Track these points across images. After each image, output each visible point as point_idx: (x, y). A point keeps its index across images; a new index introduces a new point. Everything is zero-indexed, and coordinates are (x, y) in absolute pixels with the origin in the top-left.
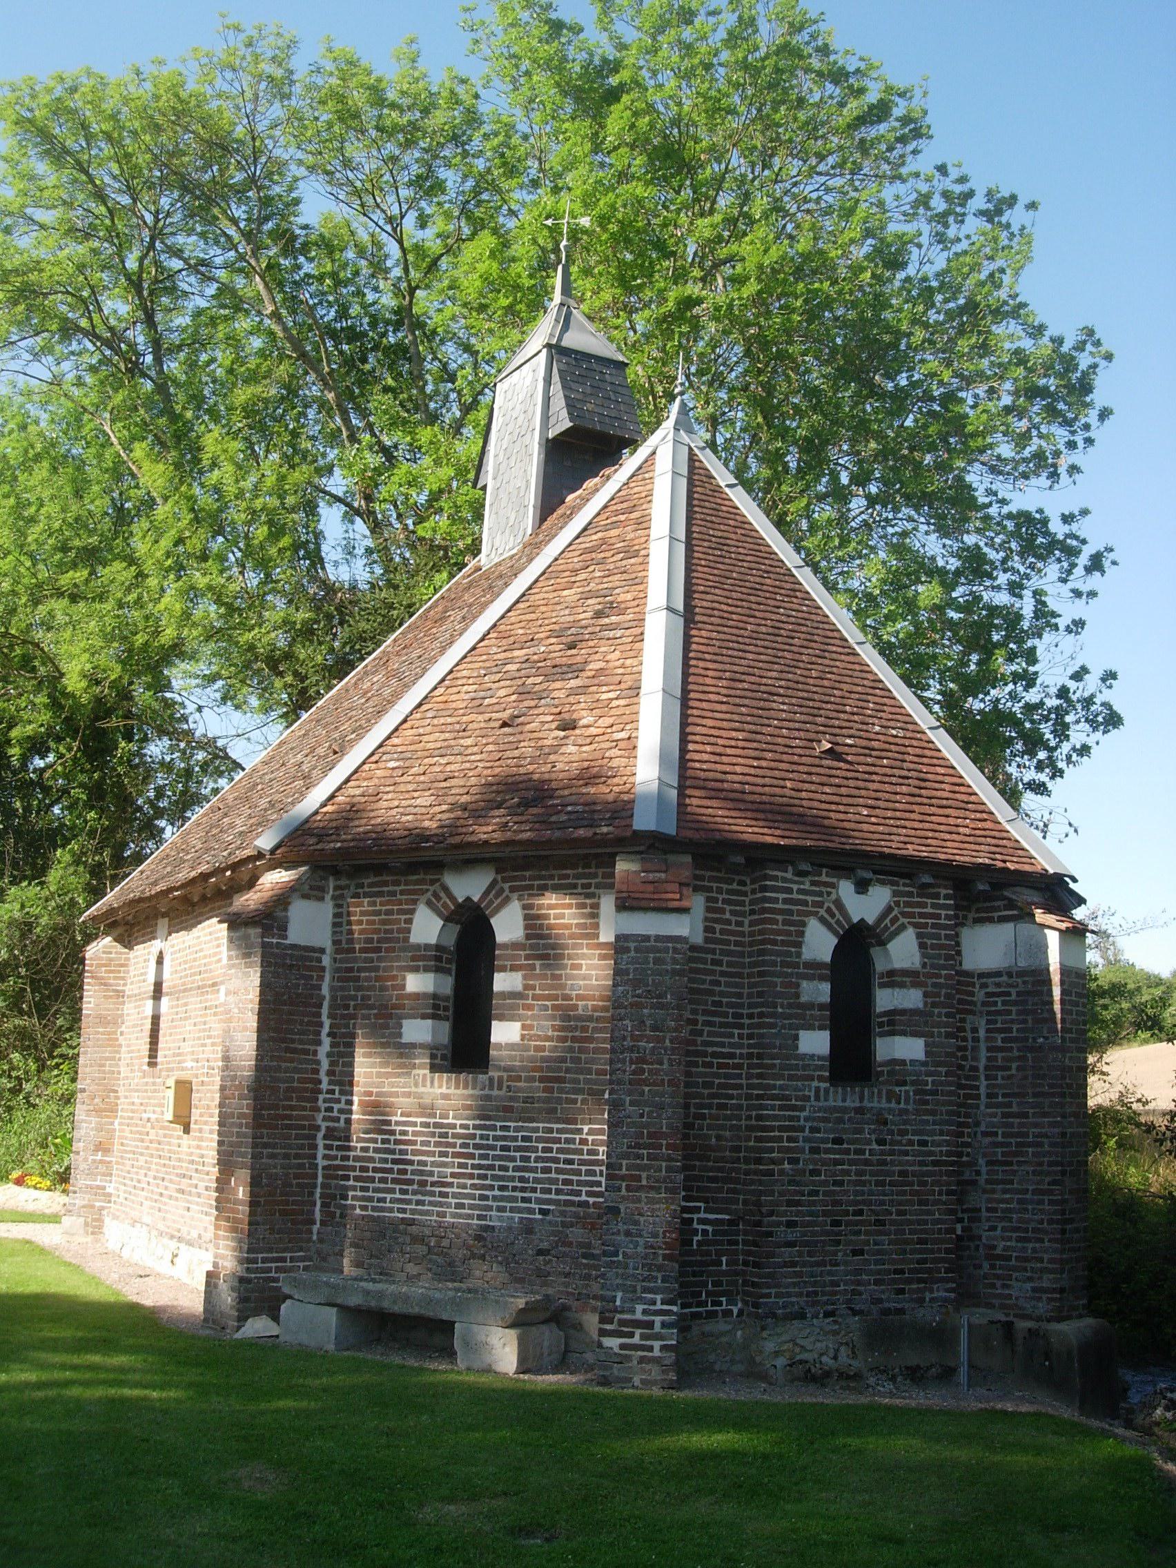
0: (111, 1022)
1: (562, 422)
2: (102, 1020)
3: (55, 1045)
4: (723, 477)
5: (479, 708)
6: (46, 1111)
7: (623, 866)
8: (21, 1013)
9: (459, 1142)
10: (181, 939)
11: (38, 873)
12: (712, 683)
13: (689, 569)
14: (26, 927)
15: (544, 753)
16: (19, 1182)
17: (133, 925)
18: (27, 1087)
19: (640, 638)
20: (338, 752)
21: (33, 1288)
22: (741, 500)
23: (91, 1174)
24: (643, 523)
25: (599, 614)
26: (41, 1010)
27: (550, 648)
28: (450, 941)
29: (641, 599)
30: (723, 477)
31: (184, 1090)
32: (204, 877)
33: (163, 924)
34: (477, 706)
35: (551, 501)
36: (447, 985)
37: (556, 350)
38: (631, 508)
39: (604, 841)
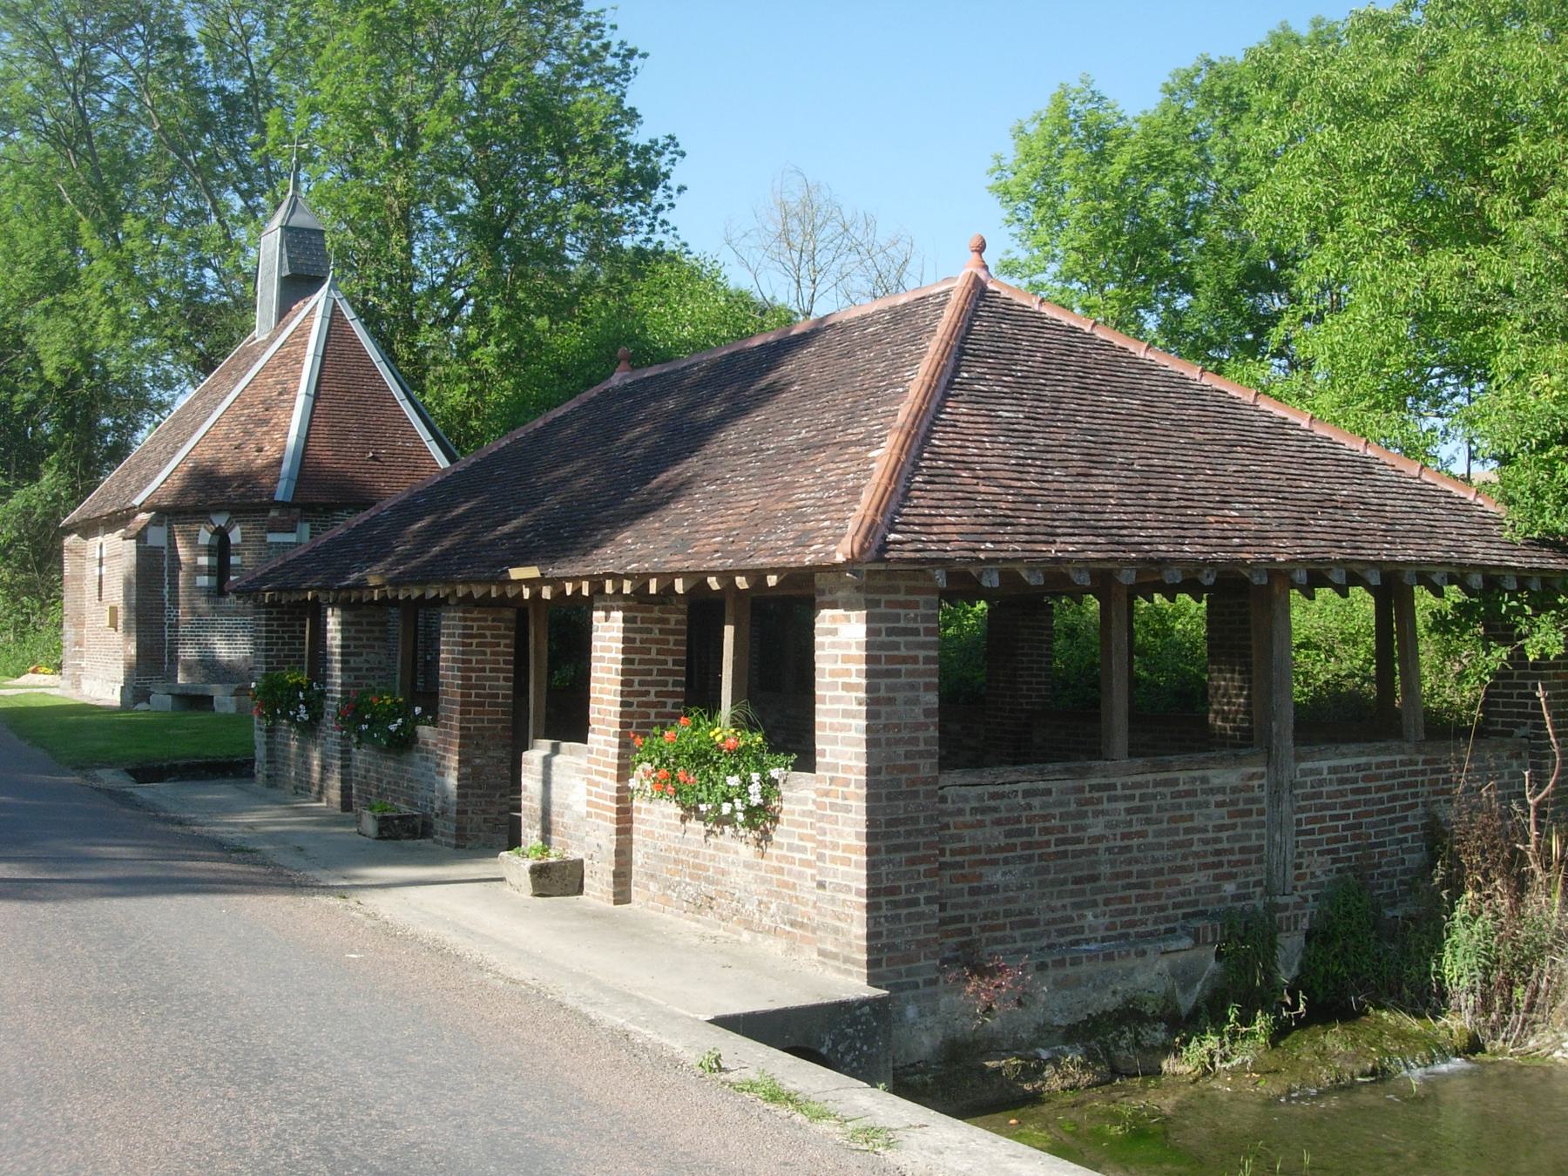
0: (80, 578)
1: (287, 273)
2: (75, 578)
3: (51, 590)
4: (349, 314)
5: (227, 438)
6: (47, 633)
7: (273, 514)
8: (27, 570)
9: (1166, 815)
10: (109, 536)
11: (35, 477)
12: (322, 429)
13: (321, 370)
14: (27, 512)
15: (250, 462)
16: (34, 672)
17: (88, 529)
18: (33, 619)
19: (292, 408)
20: (174, 453)
21: (49, 703)
22: (358, 328)
23: (73, 658)
24: (305, 344)
25: (280, 394)
26: (40, 567)
27: (258, 410)
28: (215, 543)
29: (297, 387)
30: (349, 314)
31: (113, 610)
32: (115, 513)
33: (101, 529)
34: (227, 438)
35: (284, 311)
36: (215, 561)
37: (286, 229)
38: (302, 332)
39: (265, 504)
